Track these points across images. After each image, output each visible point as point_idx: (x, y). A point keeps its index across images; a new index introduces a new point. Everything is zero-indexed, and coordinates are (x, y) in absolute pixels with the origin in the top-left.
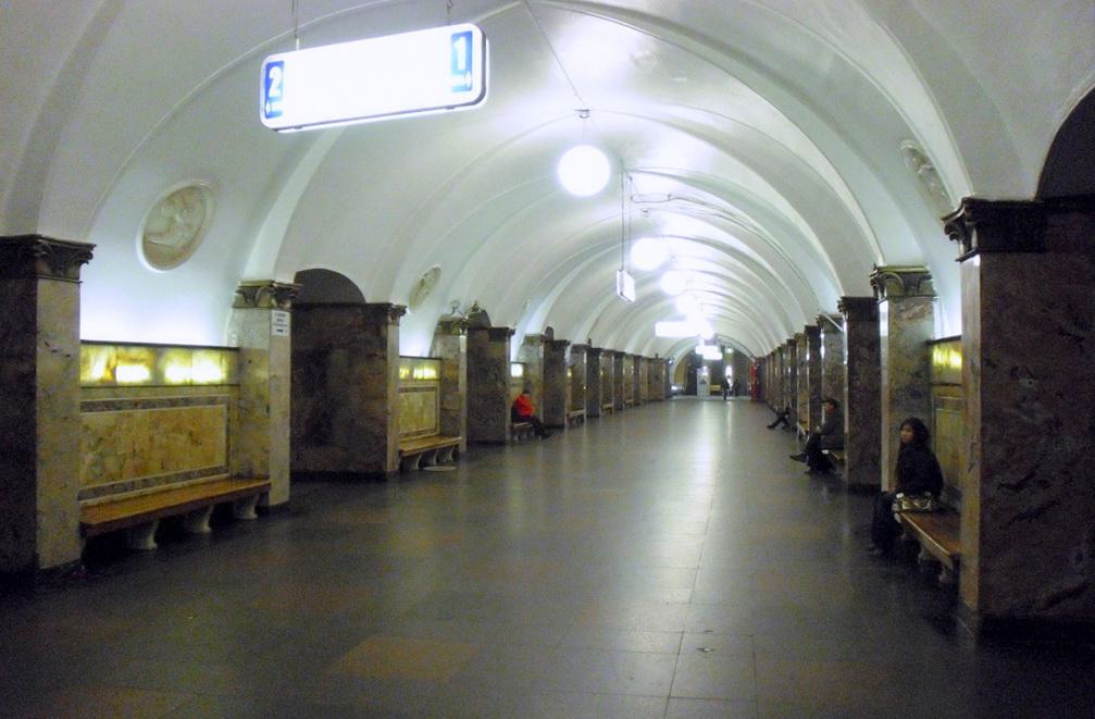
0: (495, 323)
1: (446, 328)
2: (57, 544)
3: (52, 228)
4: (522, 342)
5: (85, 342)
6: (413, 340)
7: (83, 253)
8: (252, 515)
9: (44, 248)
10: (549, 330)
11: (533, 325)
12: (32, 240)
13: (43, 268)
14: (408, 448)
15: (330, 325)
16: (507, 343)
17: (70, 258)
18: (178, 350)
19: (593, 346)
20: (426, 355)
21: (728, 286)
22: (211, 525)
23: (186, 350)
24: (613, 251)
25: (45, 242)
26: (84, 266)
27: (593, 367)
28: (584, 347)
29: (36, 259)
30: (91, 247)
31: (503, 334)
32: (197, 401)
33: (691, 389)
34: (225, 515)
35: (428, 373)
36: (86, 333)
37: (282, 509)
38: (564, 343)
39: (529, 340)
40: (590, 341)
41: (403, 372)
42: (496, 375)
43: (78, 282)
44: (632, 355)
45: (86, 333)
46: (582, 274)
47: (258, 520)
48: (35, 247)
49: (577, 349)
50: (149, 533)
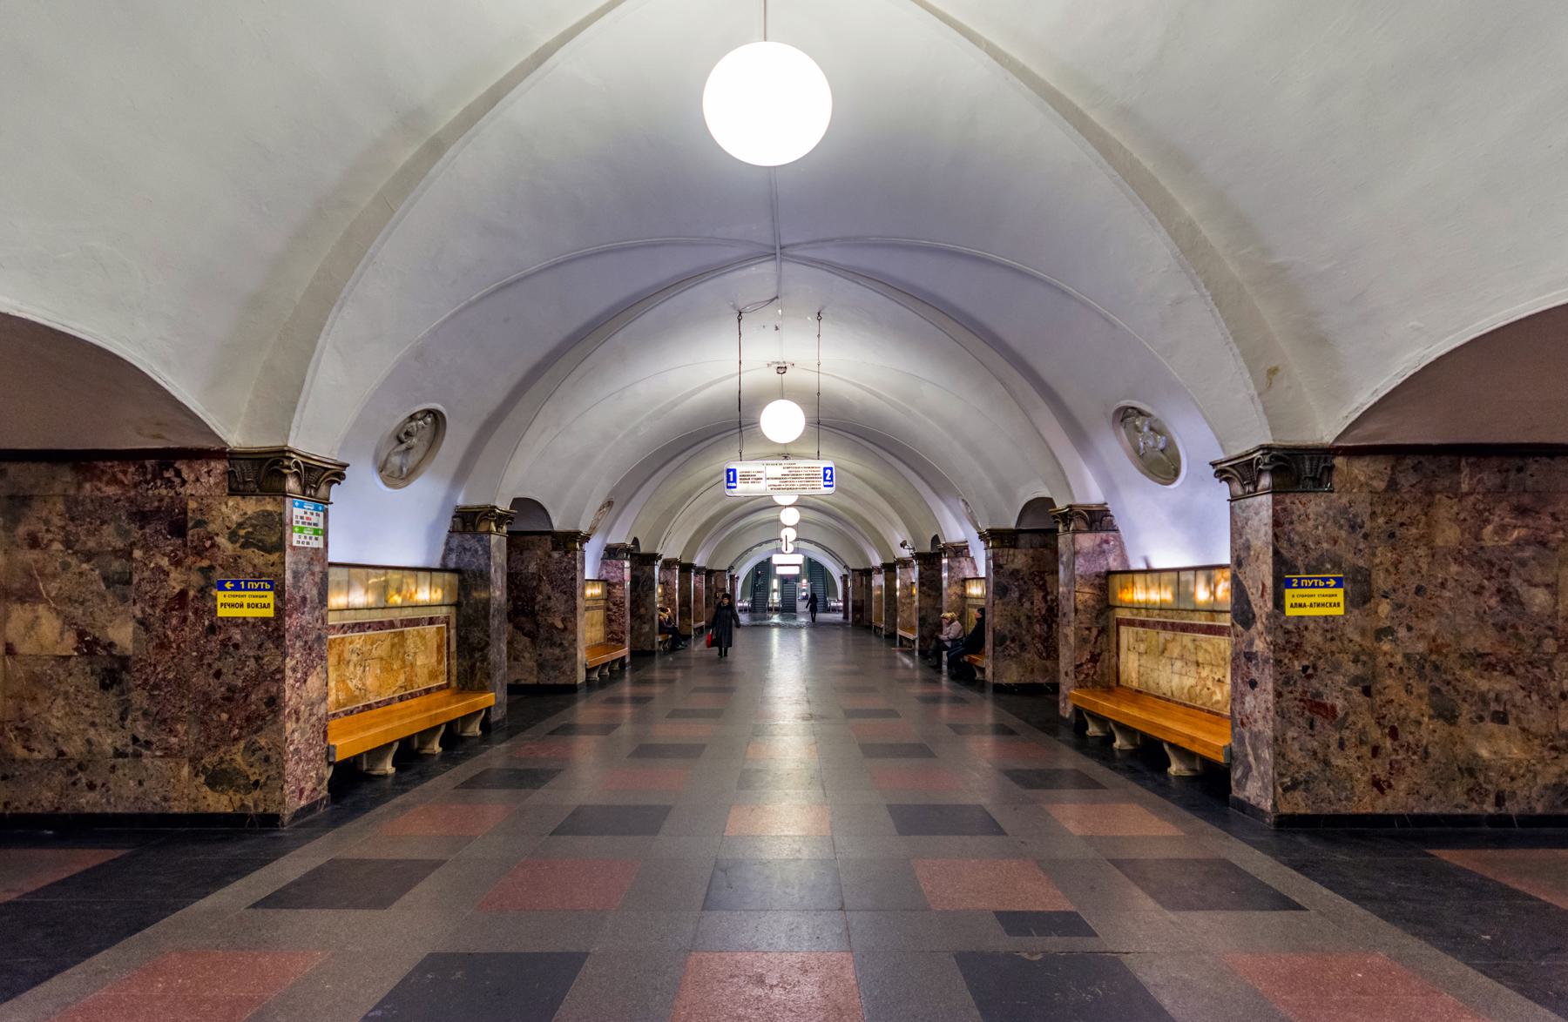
0: (558, 524)
2: (303, 781)
4: (447, 526)
5: (331, 564)
11: (620, 537)
12: (282, 454)
13: (292, 484)
14: (347, 744)
19: (643, 550)
24: (740, 530)
25: (299, 459)
27: (641, 585)
28: (628, 551)
29: (285, 476)
31: (570, 541)
33: (759, 607)
38: (653, 557)
39: (612, 553)
40: (636, 541)
44: (1018, 685)
46: (732, 538)
47: (443, 757)
49: (668, 565)
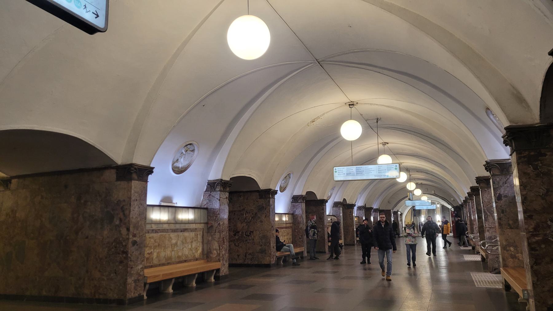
1: (295, 199)
3: (139, 160)
6: (281, 205)
7: (150, 170)
8: (213, 280)
9: (135, 169)
10: (344, 200)
13: (134, 176)
15: (244, 196)
16: (271, 200)
17: (145, 172)
18: (184, 209)
20: (158, 204)
21: (427, 178)
22: (173, 289)
23: (186, 209)
25: (136, 167)
26: (150, 176)
29: (132, 173)
30: (153, 168)
31: (352, 206)
32: (164, 231)
34: (202, 279)
35: (285, 218)
36: (149, 203)
37: (226, 277)
38: (352, 206)
41: (277, 219)
42: (121, 220)
43: (146, 181)
45: (149, 203)
48: (132, 169)
50: (170, 285)
